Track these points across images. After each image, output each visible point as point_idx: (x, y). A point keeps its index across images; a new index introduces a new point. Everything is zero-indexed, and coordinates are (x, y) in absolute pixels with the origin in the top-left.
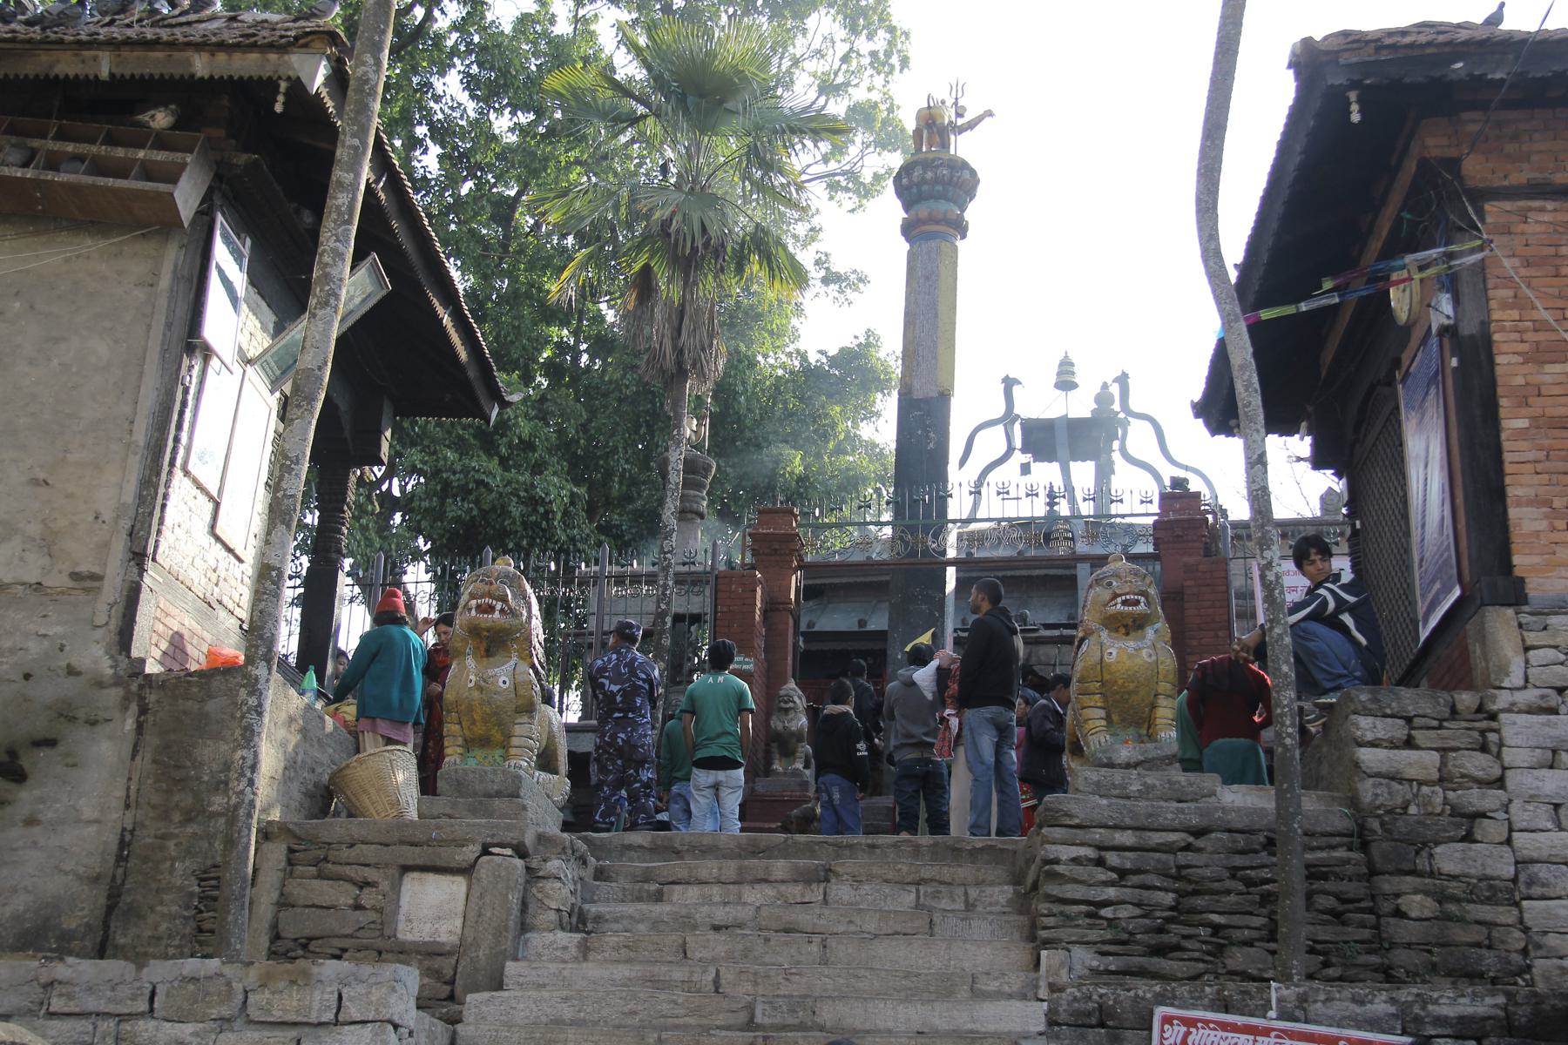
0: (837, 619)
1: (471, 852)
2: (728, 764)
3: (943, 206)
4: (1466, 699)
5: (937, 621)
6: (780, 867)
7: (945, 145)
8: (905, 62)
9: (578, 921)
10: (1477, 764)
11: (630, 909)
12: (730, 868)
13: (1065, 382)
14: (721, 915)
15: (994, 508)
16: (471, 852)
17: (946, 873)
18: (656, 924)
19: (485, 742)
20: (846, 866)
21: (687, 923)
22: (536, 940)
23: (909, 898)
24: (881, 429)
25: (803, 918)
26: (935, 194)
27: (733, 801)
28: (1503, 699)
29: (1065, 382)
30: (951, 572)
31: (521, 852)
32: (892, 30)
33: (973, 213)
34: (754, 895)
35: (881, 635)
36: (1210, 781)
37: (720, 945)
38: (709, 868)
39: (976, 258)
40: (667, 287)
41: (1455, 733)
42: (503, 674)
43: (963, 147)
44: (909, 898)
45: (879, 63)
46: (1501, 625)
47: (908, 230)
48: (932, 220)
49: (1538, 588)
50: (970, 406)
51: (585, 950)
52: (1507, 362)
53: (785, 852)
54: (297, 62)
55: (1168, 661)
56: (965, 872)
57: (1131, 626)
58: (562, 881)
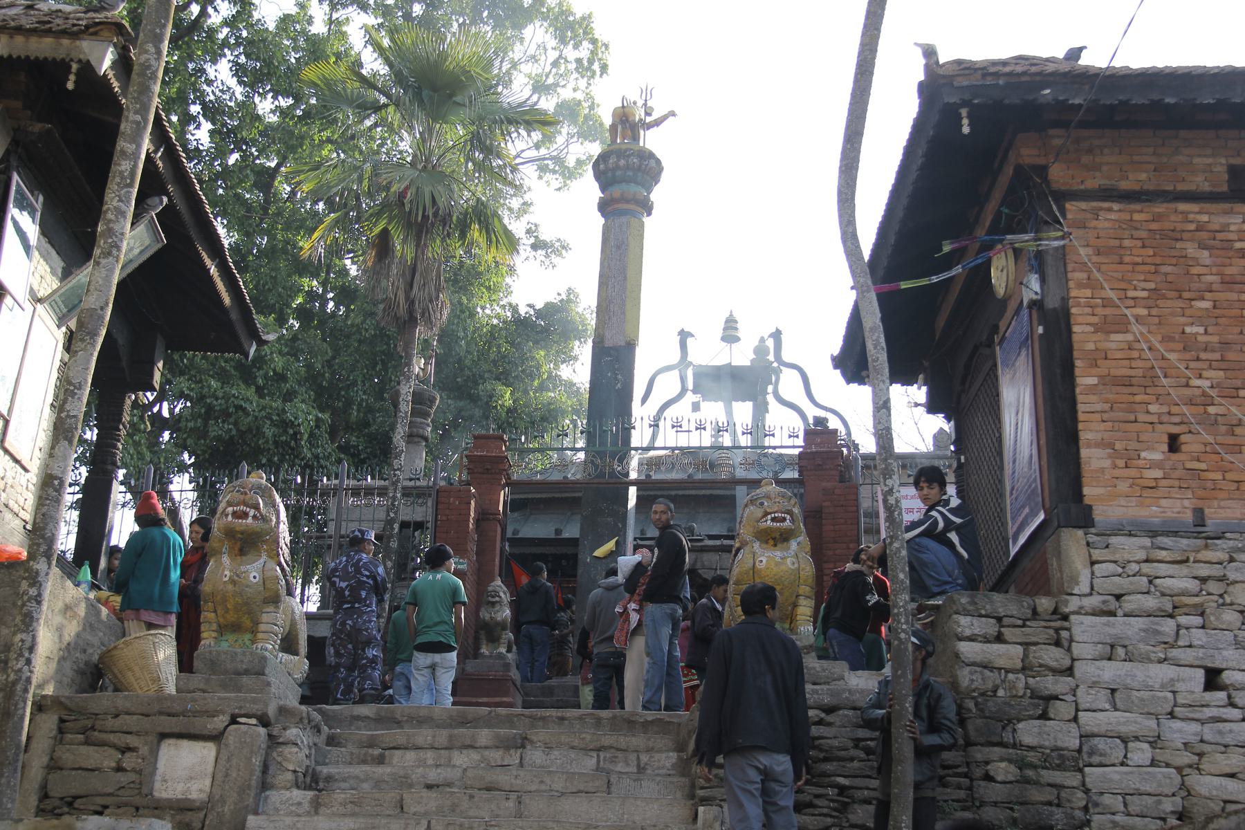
0: (538, 528)
1: (221, 721)
2: (444, 648)
3: (633, 189)
4: (1044, 603)
5: (620, 532)
6: (484, 736)
7: (636, 138)
8: (604, 68)
9: (312, 781)
10: (1052, 656)
11: (358, 770)
12: (442, 736)
13: (730, 333)
14: (433, 776)
15: (669, 438)
16: (221, 721)
17: (622, 741)
18: (378, 784)
19: (236, 628)
20: (540, 735)
21: (404, 782)
22: (275, 797)
23: (591, 762)
24: (577, 370)
25: (503, 778)
26: (626, 178)
27: (447, 680)
28: (1073, 604)
29: (730, 333)
30: (633, 491)
31: (264, 722)
32: (594, 41)
33: (657, 195)
34: (461, 759)
35: (574, 542)
36: (841, 667)
37: (432, 801)
38: (424, 736)
39: (659, 233)
40: (402, 247)
41: (1036, 631)
42: (253, 571)
43: (651, 140)
44: (591, 762)
45: (583, 68)
46: (1073, 543)
47: (604, 207)
48: (623, 199)
49: (1105, 513)
50: (652, 354)
51: (316, 806)
52: (1082, 332)
53: (488, 723)
54: (87, 47)
55: (808, 569)
56: (637, 741)
57: (778, 538)
58: (299, 746)
